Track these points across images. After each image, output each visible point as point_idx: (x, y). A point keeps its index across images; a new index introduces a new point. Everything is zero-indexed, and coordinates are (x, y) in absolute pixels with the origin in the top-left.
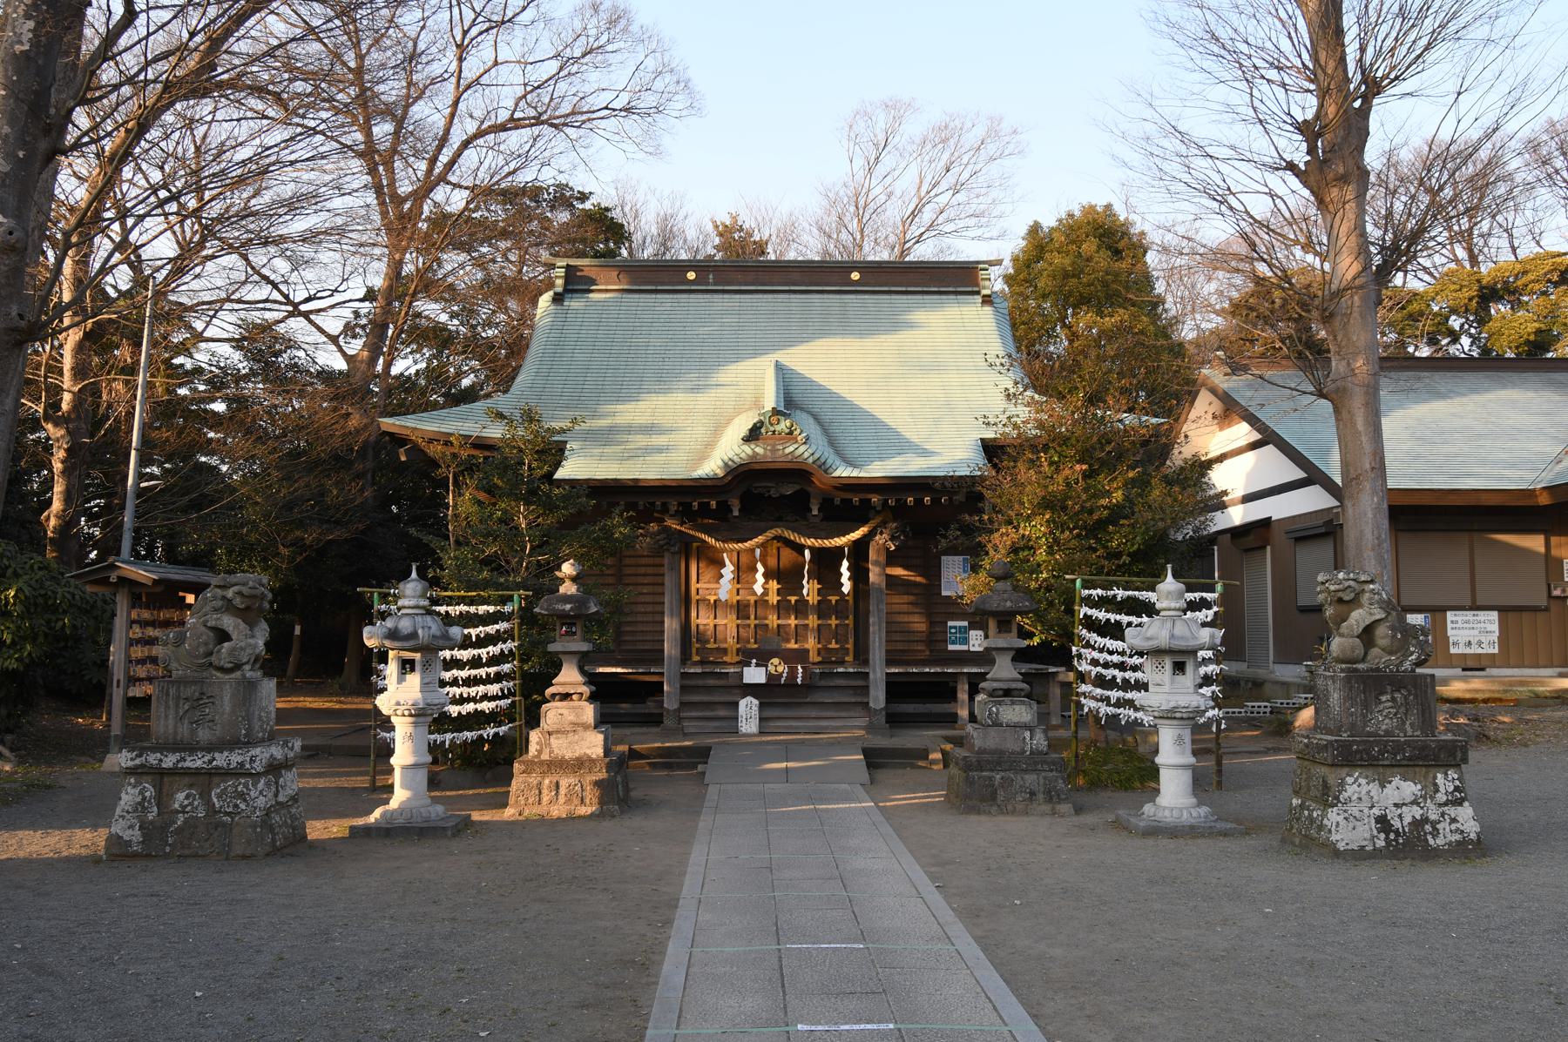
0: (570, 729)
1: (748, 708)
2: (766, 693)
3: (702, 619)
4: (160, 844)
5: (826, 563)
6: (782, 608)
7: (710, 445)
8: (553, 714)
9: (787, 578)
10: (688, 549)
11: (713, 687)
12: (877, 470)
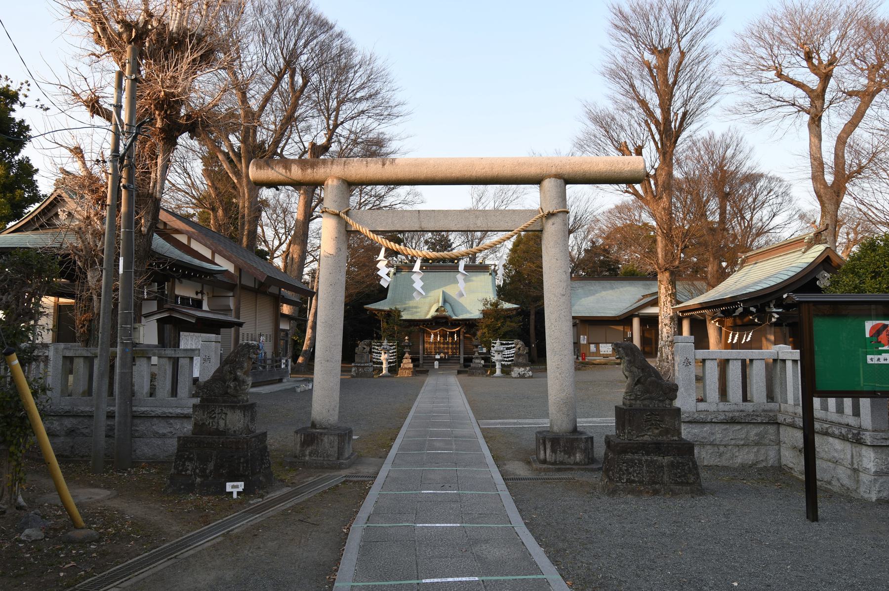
0: (407, 363)
1: (436, 363)
2: (441, 360)
3: (427, 346)
4: (358, 375)
5: (452, 334)
6: (444, 343)
7: (429, 311)
8: (404, 361)
9: (444, 336)
10: (424, 332)
11: (430, 360)
12: (461, 317)
